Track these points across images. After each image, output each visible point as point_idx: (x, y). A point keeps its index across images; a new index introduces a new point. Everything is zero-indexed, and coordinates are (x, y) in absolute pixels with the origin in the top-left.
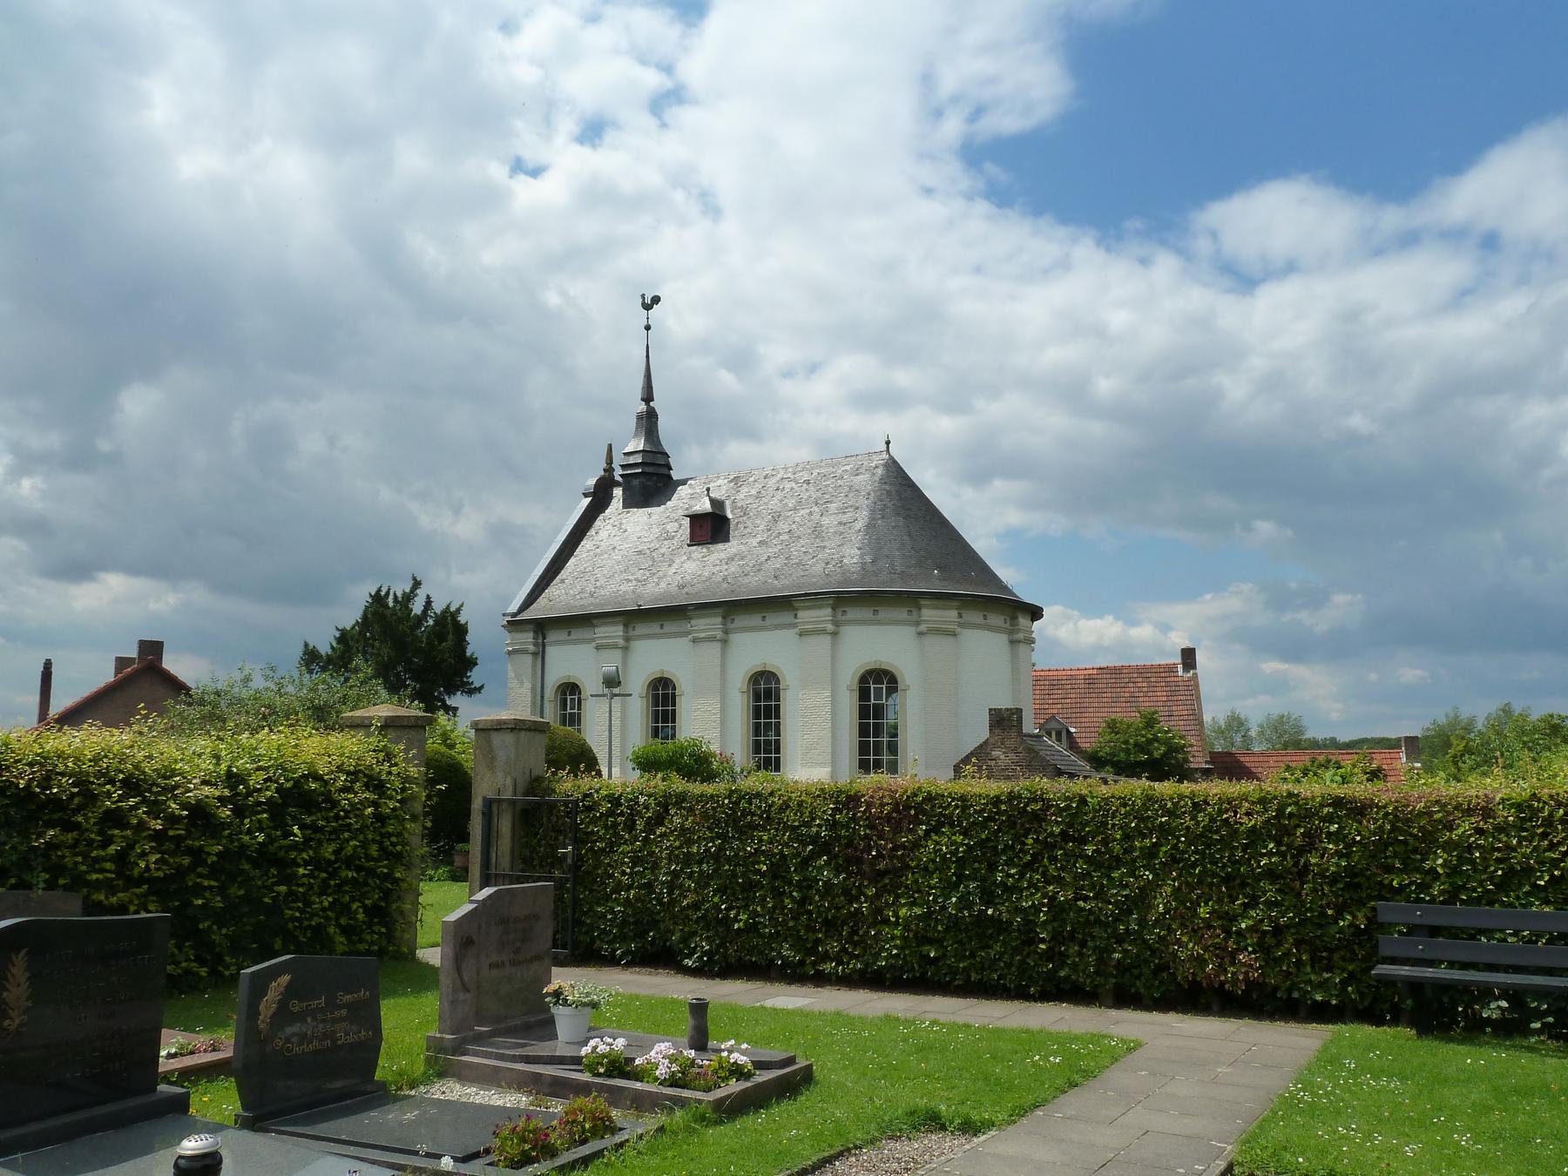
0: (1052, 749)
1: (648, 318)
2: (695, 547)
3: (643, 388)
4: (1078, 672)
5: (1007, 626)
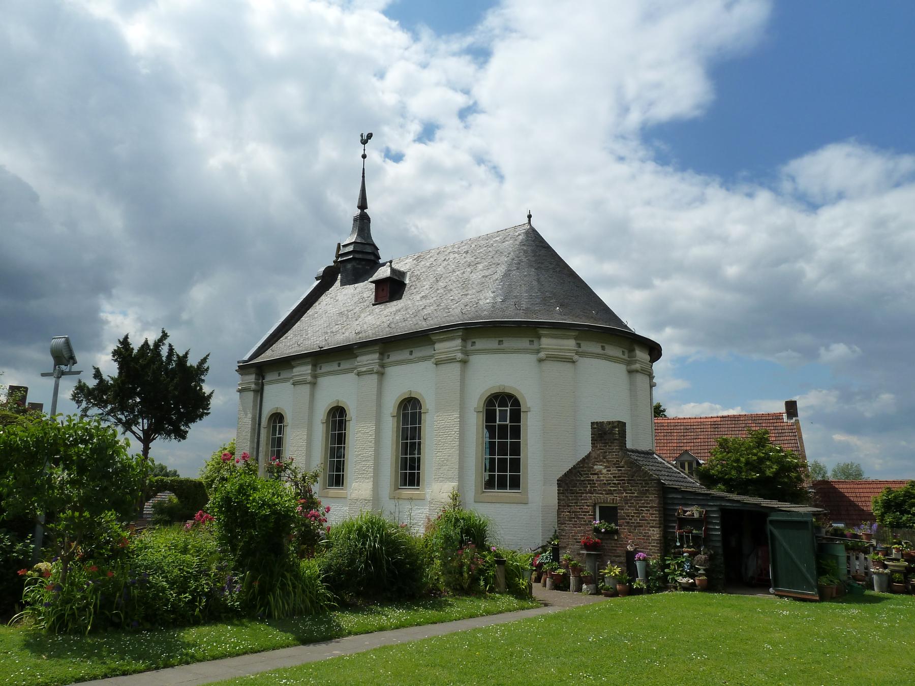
0: (669, 470)
1: (364, 150)
2: (377, 306)
3: (359, 199)
4: (706, 420)
5: (626, 357)
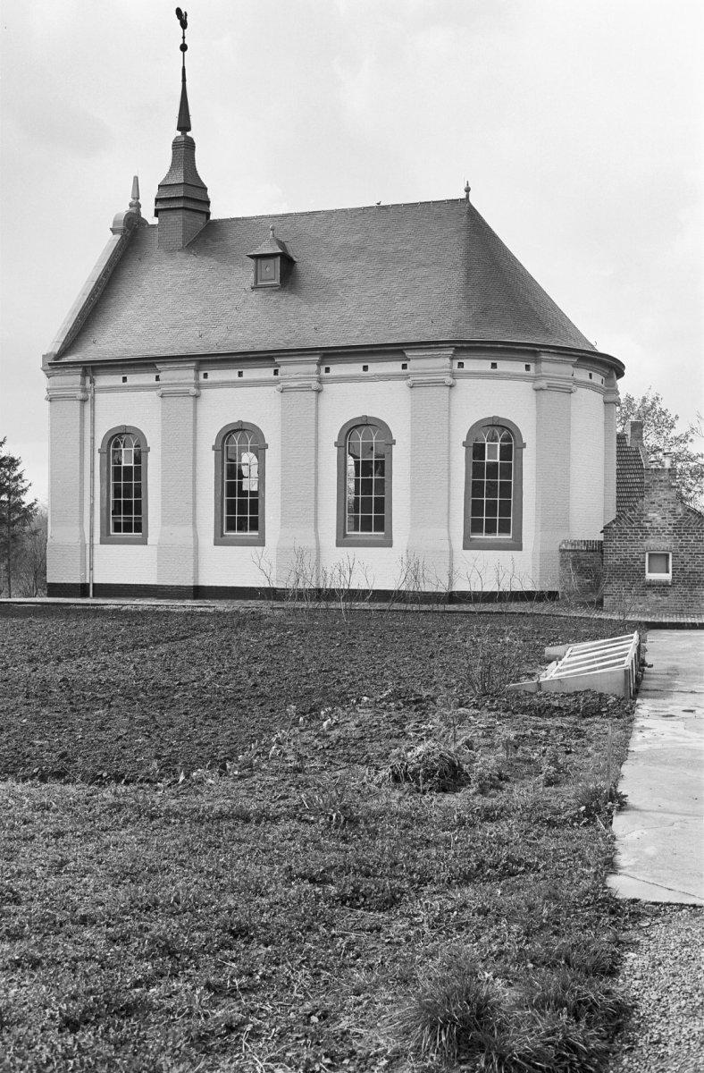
1: (184, 38)
